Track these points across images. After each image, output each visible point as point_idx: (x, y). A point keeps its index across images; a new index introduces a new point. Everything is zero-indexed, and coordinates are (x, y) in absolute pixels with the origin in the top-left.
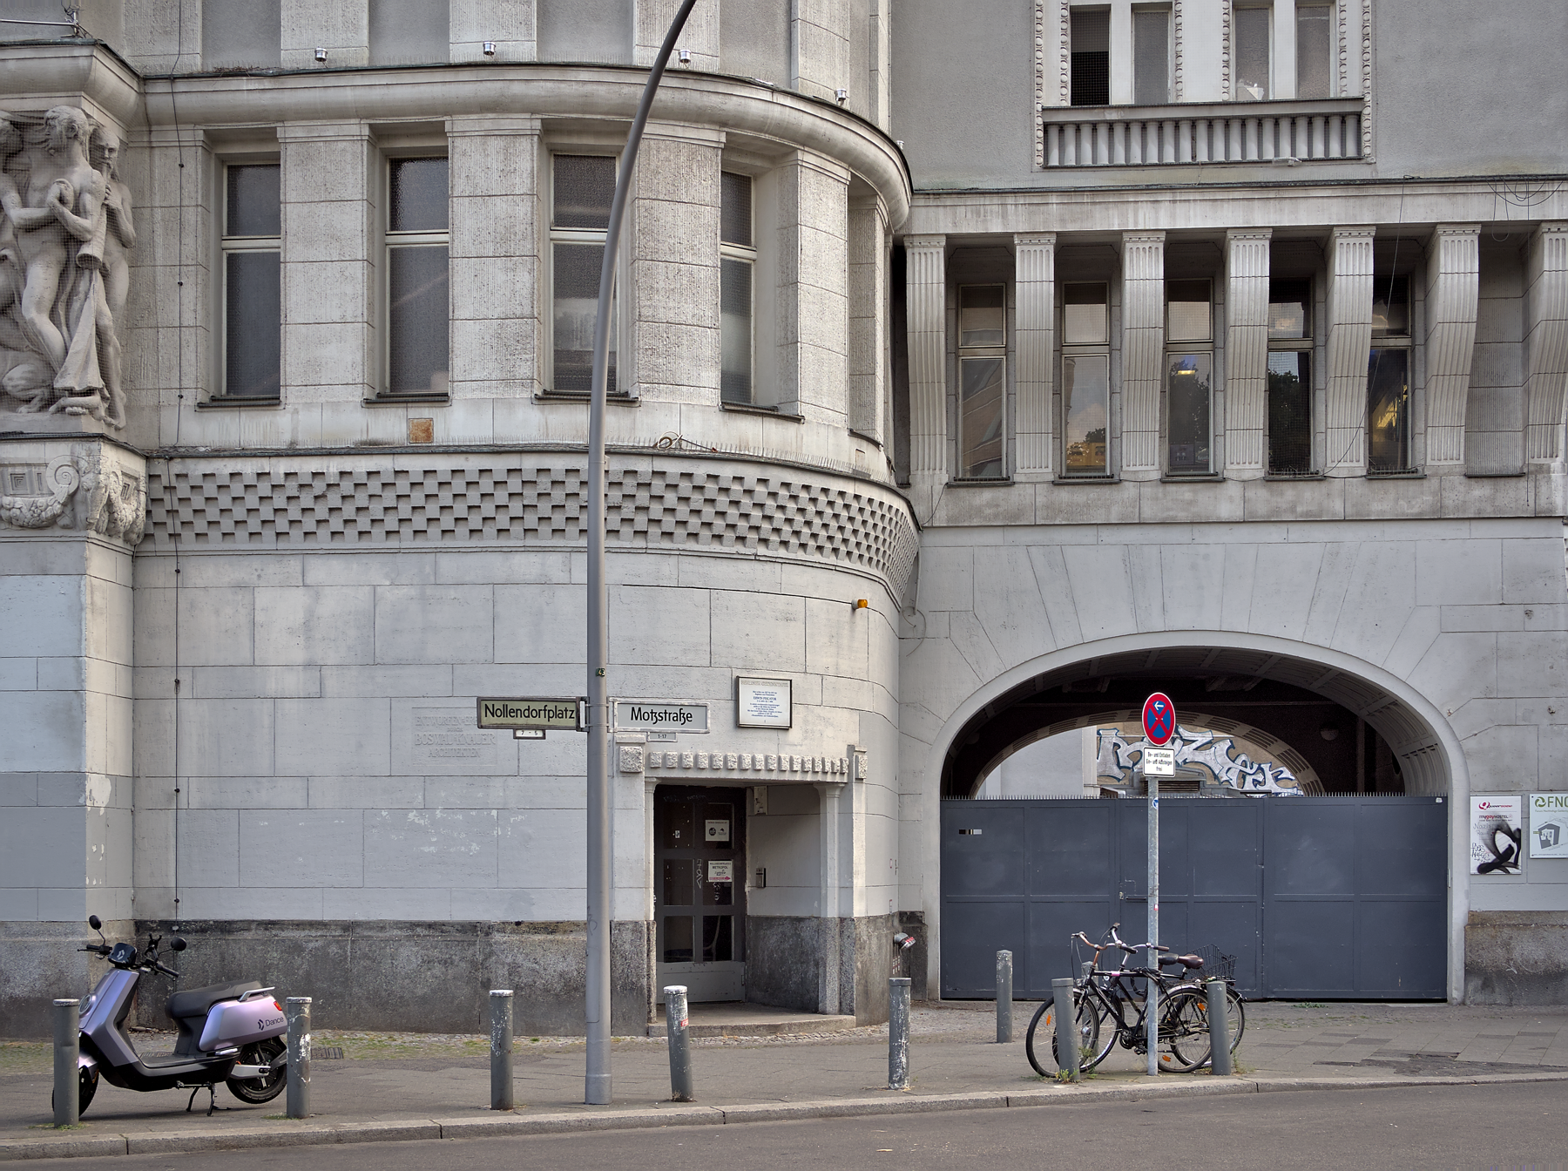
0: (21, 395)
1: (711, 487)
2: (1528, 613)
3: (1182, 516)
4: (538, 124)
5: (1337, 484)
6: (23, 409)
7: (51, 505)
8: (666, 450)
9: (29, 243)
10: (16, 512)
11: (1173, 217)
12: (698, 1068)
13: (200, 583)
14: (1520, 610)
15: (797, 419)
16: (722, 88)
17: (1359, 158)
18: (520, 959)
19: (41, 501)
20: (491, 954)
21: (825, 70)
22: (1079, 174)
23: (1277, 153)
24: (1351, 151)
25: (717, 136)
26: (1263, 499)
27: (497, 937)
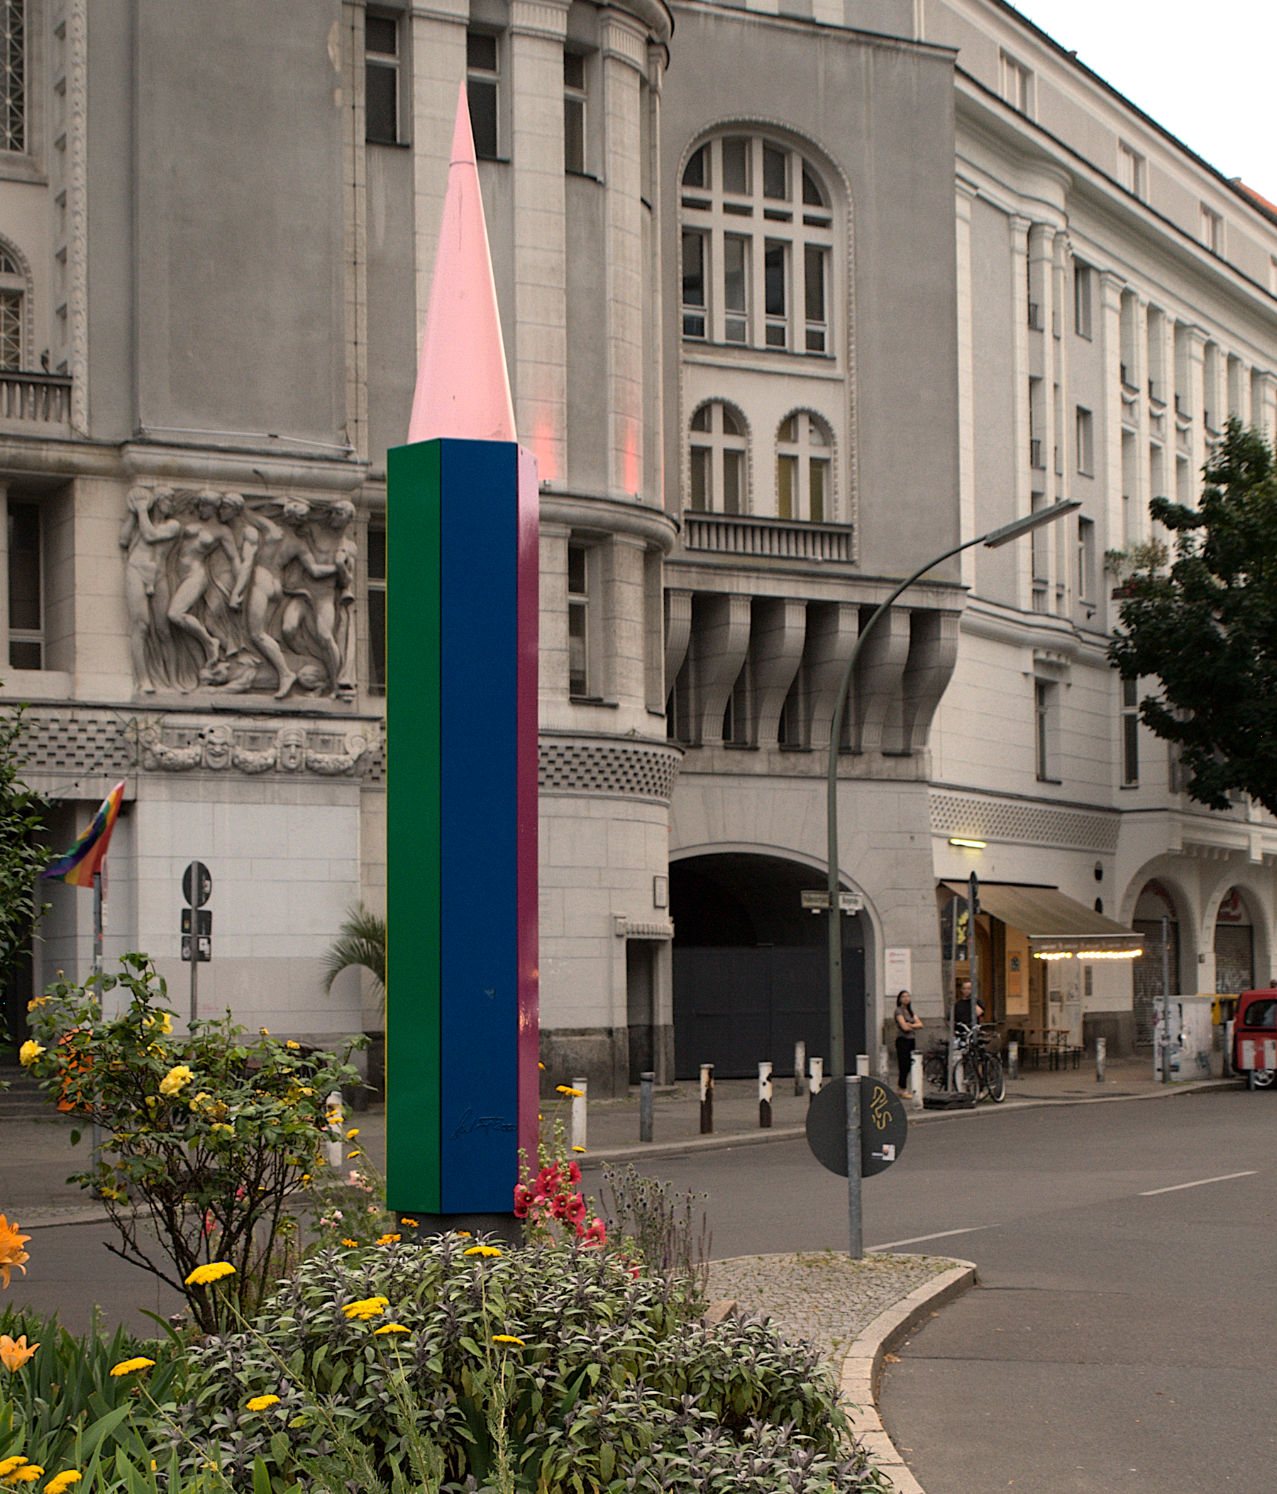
0: (311, 686)
1: (598, 755)
2: (912, 838)
3: (735, 770)
4: (569, 532)
5: (817, 755)
6: (311, 694)
7: (348, 761)
8: (630, 738)
9: (320, 588)
10: (323, 764)
11: (758, 587)
12: (719, 1111)
13: (371, 809)
14: (908, 836)
15: (614, 707)
16: (654, 517)
17: (850, 562)
18: (568, 1052)
19: (342, 758)
20: (552, 1049)
21: (629, 487)
22: (698, 554)
23: (788, 551)
24: (844, 558)
25: (642, 544)
26: (779, 763)
27: (554, 1038)
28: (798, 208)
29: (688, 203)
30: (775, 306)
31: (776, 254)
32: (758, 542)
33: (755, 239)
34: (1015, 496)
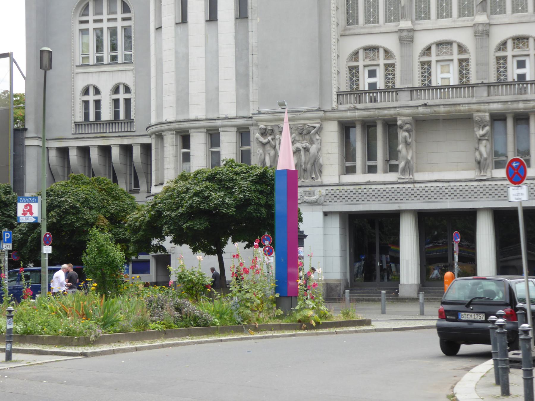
25: (236, 129)
28: (119, 15)
29: (82, 22)
30: (114, 47)
31: (113, 32)
32: (111, 127)
33: (90, 30)
34: (9, 119)
